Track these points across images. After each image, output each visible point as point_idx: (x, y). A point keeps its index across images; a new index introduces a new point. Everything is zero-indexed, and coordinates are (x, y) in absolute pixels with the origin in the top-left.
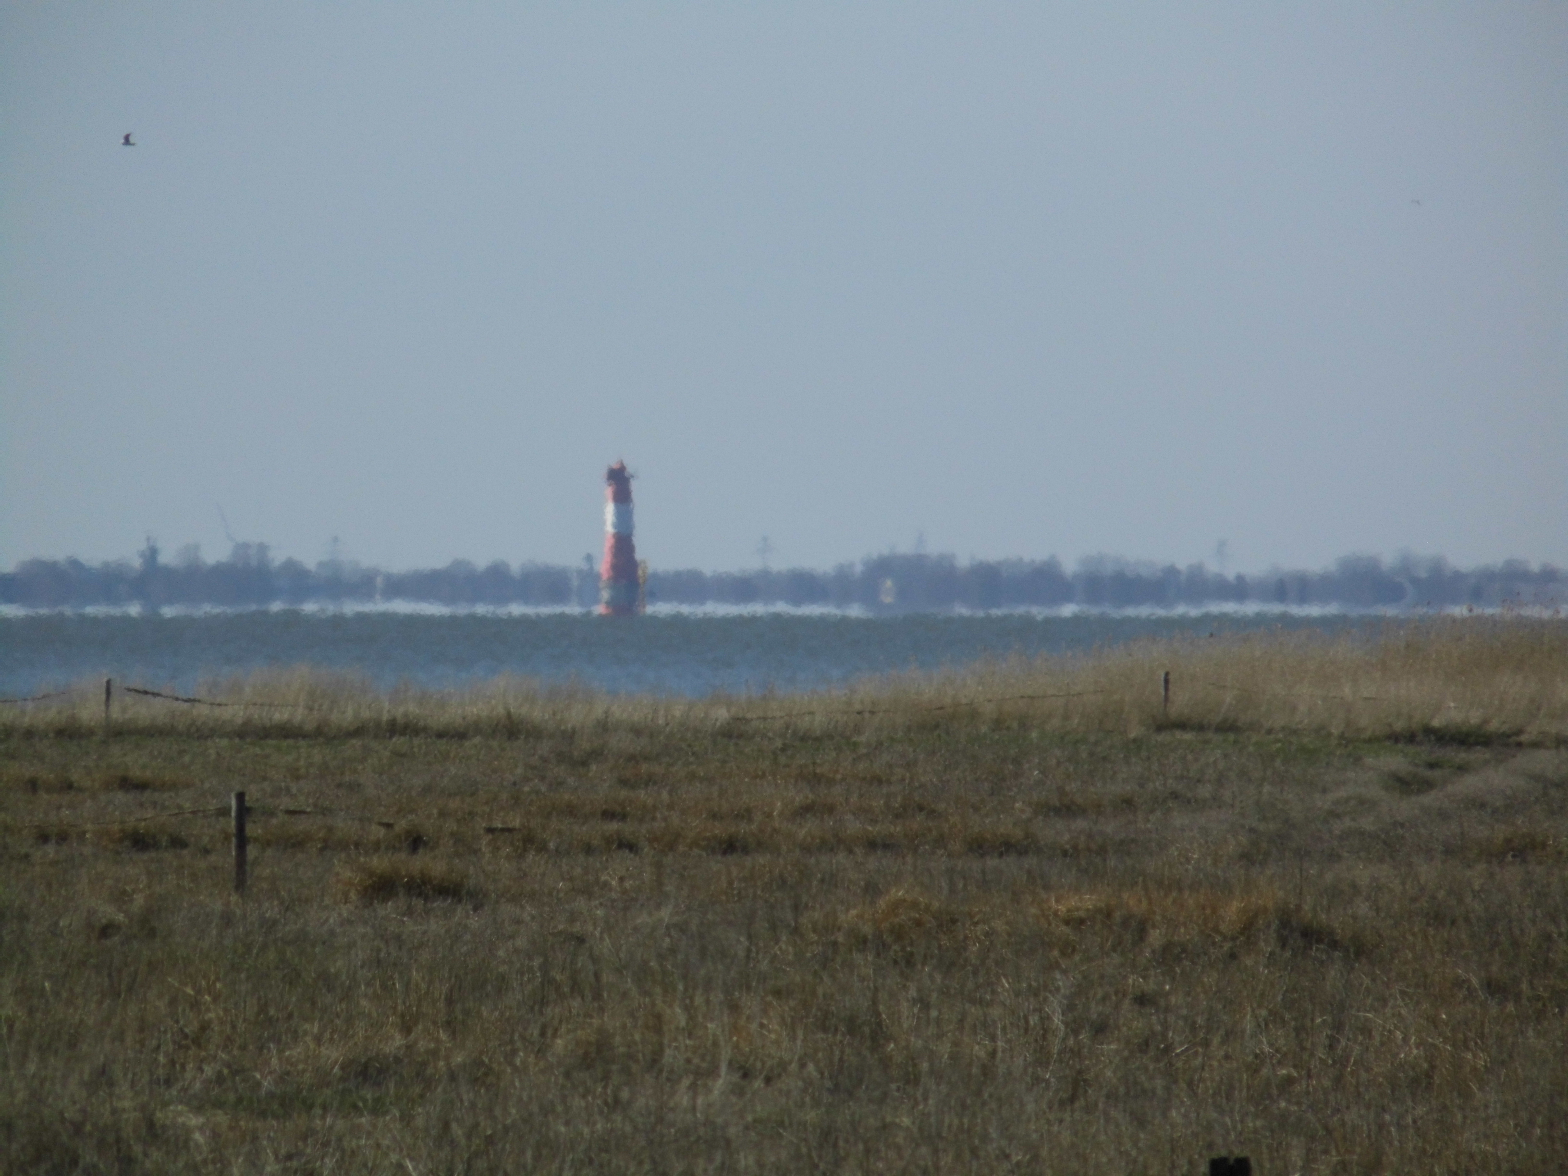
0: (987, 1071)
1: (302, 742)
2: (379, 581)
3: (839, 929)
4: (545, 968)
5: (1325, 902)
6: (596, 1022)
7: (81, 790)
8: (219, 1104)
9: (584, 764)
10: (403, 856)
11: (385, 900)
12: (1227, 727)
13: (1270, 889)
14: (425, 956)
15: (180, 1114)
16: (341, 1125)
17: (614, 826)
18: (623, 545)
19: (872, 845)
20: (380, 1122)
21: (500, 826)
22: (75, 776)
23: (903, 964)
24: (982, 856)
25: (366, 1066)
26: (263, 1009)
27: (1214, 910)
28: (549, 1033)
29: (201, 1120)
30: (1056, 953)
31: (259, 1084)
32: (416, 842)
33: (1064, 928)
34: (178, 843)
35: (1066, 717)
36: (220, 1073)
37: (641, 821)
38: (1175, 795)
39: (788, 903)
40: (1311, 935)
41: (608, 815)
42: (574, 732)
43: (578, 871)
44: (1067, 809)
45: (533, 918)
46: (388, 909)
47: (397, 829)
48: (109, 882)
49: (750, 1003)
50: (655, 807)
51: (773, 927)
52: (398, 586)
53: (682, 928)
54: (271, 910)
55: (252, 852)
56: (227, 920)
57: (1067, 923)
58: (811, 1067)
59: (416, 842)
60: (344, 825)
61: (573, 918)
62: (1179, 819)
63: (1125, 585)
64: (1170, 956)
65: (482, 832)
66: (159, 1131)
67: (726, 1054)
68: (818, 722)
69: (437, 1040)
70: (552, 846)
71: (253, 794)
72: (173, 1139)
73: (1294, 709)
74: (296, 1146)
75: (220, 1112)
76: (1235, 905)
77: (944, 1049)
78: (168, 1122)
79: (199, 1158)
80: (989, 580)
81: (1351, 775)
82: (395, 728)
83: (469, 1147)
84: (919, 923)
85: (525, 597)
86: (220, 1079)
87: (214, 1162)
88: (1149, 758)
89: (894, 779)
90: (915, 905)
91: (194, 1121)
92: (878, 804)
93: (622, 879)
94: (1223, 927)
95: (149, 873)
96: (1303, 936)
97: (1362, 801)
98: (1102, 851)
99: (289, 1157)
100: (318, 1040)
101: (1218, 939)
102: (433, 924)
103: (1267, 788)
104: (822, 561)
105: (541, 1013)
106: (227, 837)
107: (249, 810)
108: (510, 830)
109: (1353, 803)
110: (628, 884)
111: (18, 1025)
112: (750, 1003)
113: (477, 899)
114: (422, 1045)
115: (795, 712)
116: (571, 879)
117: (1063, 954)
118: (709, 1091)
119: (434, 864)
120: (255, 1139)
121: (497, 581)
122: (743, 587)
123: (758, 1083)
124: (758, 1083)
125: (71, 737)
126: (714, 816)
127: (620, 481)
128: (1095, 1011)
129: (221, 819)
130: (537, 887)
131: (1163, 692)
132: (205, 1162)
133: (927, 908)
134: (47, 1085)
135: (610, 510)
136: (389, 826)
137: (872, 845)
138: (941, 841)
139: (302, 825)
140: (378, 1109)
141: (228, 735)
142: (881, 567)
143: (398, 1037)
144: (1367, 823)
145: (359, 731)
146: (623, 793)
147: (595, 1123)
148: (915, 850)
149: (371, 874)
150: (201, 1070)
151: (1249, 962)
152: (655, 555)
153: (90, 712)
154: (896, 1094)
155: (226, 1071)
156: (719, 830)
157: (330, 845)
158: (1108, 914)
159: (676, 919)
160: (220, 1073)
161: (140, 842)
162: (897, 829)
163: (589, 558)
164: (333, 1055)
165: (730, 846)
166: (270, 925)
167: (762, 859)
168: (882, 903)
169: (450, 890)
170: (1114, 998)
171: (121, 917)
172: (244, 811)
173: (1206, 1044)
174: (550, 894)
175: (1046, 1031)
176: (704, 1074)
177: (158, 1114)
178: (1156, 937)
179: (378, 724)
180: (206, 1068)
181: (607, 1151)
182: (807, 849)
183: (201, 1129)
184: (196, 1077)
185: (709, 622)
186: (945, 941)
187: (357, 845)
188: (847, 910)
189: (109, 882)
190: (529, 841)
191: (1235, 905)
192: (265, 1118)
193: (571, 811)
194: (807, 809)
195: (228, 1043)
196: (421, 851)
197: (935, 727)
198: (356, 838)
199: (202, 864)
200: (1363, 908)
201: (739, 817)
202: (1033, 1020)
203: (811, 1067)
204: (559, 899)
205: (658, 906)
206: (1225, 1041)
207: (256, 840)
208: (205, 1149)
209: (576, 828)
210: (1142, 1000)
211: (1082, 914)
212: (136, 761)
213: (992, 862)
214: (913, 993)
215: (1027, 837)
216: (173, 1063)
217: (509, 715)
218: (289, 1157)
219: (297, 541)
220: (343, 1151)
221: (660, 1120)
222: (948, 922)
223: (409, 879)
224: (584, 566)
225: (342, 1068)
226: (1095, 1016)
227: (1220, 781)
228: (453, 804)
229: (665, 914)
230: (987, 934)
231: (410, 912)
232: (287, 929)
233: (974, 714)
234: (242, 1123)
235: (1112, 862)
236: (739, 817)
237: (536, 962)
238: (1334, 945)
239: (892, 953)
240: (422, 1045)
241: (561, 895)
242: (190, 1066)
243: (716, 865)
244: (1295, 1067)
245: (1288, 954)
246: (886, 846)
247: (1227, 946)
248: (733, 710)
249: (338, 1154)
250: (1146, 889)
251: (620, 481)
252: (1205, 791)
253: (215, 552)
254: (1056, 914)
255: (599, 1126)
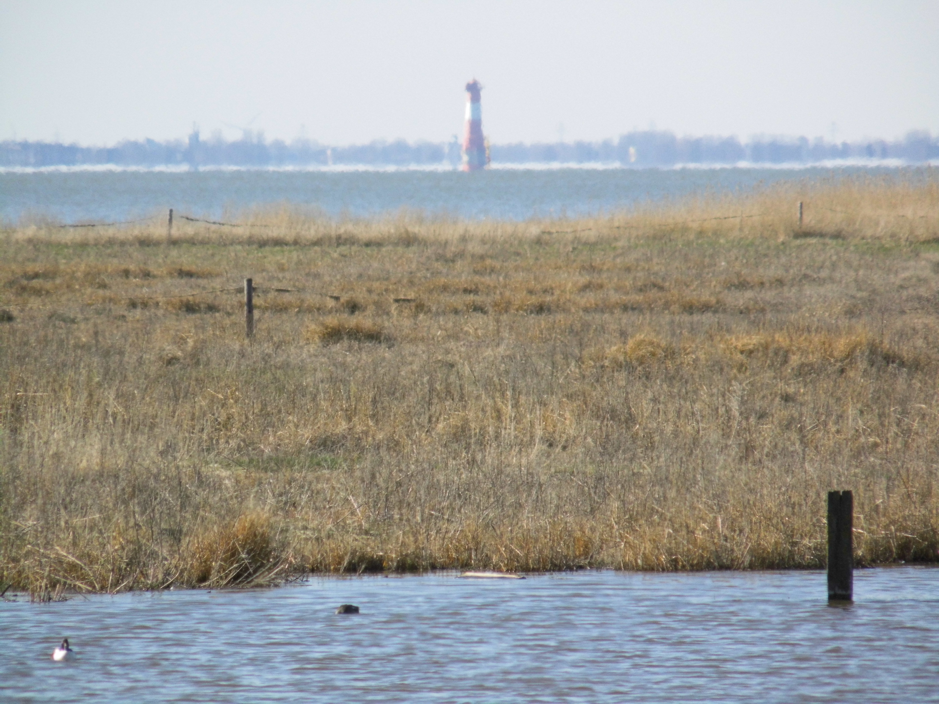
0: (695, 441)
1: (285, 248)
2: (329, 152)
3: (606, 358)
4: (431, 382)
5: (896, 339)
6: (462, 414)
7: (154, 277)
8: (239, 464)
9: (453, 261)
10: (346, 315)
11: (336, 343)
12: (837, 235)
13: (863, 331)
14: (359, 374)
15: (217, 469)
16: (310, 476)
17: (471, 297)
18: (476, 126)
19: (625, 308)
20: (335, 473)
21: (403, 297)
22: (152, 268)
23: (644, 379)
24: (691, 314)
25: (325, 440)
26: (264, 406)
27: (830, 345)
28: (434, 419)
29: (229, 473)
30: (735, 371)
31: (263, 451)
32: (353, 307)
33: (739, 355)
34: (212, 308)
35: (741, 229)
36: (239, 445)
37: (487, 294)
38: (806, 276)
39: (575, 343)
40: (889, 359)
41: (466, 291)
42: (446, 243)
43: (450, 325)
44: (743, 285)
45: (424, 352)
46: (337, 348)
47: (342, 300)
48: (172, 332)
49: (553, 401)
50: (495, 287)
51: (566, 358)
52: (341, 156)
53: (512, 358)
54: (268, 348)
55: (256, 314)
56: (242, 354)
57: (742, 352)
58: (589, 440)
59: (353, 307)
60: (311, 299)
61: (447, 352)
62: (808, 290)
63: (776, 150)
64: (803, 372)
65: (392, 301)
66: (204, 480)
67: (539, 432)
68: (592, 235)
69: (367, 425)
70: (434, 309)
71: (257, 281)
72: (212, 484)
73: (877, 224)
74: (285, 487)
75: (240, 468)
76: (842, 341)
77: (669, 429)
78: (209, 474)
79: (228, 496)
80: (696, 149)
81: (912, 263)
82: (340, 241)
83: (387, 488)
84: (653, 354)
85: (418, 161)
86: (239, 449)
87: (236, 497)
88: (790, 254)
89: (639, 268)
90: (651, 343)
91: (224, 473)
92: (628, 283)
93: (476, 329)
94: (836, 354)
95: (196, 327)
96: (883, 360)
97: (919, 280)
98: (763, 310)
99: (281, 495)
100: (297, 426)
101: (832, 360)
102: (365, 356)
103: (861, 272)
104: (594, 136)
105: (429, 409)
106: (241, 306)
107: (254, 289)
108: (409, 301)
109: (914, 280)
110: (480, 332)
111: (119, 417)
112: (553, 401)
113: (390, 341)
114: (359, 428)
115: (579, 228)
116: (446, 330)
117: (739, 371)
118: (528, 456)
119: (364, 320)
120: (260, 484)
121: (399, 150)
122: (549, 152)
123: (558, 449)
124: (558, 449)
125: (148, 246)
126: (531, 292)
127: (474, 90)
128: (758, 404)
129: (238, 295)
130: (425, 334)
131: (798, 215)
132: (231, 498)
133: (659, 346)
134: (138, 453)
135: (468, 106)
136: (337, 298)
137: (625, 308)
138: (667, 305)
139: (287, 298)
140: (332, 466)
141: (240, 243)
142: (630, 139)
143: (344, 423)
144: (923, 291)
145: (318, 243)
146: (477, 278)
147: (461, 474)
148: (652, 310)
149: (327, 328)
150: (227, 442)
151: (852, 374)
152: (494, 135)
153: (159, 231)
154: (642, 455)
155: (242, 444)
156: (534, 300)
157: (303, 310)
158: (766, 347)
159: (508, 353)
160: (239, 445)
161: (190, 308)
162: (640, 298)
163: (456, 137)
164: (306, 434)
165: (540, 309)
166: (266, 358)
167: (560, 317)
168: (631, 343)
169: (374, 336)
170: (770, 397)
171: (180, 353)
172: (251, 289)
173: (825, 424)
174: (433, 338)
175: (729, 418)
176: (524, 445)
177: (203, 469)
178: (795, 360)
179: (330, 238)
180: (230, 441)
181: (468, 490)
182: (586, 310)
183: (229, 478)
184: (227, 446)
185: (528, 173)
186: (669, 363)
187: (319, 309)
188: (610, 347)
189: (172, 332)
190: (420, 307)
191: (842, 341)
192: (266, 472)
193: (445, 288)
194: (586, 287)
195: (244, 426)
196: (357, 313)
197: (661, 239)
198: (318, 305)
199: (227, 322)
200: (920, 343)
201: (545, 291)
202: (722, 410)
203: (589, 440)
204: (439, 341)
205: (498, 345)
206: (836, 423)
207: (259, 307)
208: (232, 490)
209: (448, 299)
210: (787, 398)
211: (751, 347)
212: (186, 259)
213: (696, 317)
214: (650, 395)
215: (718, 302)
216: (211, 439)
217: (407, 232)
218: (281, 495)
219: (279, 130)
220: (313, 492)
221: (500, 472)
222: (670, 353)
223: (350, 331)
224: (453, 140)
225: (311, 442)
226: (758, 408)
227: (834, 266)
228: (376, 285)
229: (501, 350)
230: (694, 361)
231: (350, 349)
232: (278, 359)
233: (685, 229)
234: (253, 474)
235: (769, 316)
236: (545, 291)
237: (426, 379)
238: (902, 364)
239: (637, 372)
240: (359, 428)
241: (440, 339)
242: (222, 441)
243: (532, 319)
244: (878, 436)
245: (874, 369)
246: (633, 309)
247: (839, 364)
248: (542, 227)
249: (309, 493)
250: (788, 332)
251: (474, 90)
252: (824, 274)
253: (232, 136)
254: (736, 348)
255: (464, 476)
